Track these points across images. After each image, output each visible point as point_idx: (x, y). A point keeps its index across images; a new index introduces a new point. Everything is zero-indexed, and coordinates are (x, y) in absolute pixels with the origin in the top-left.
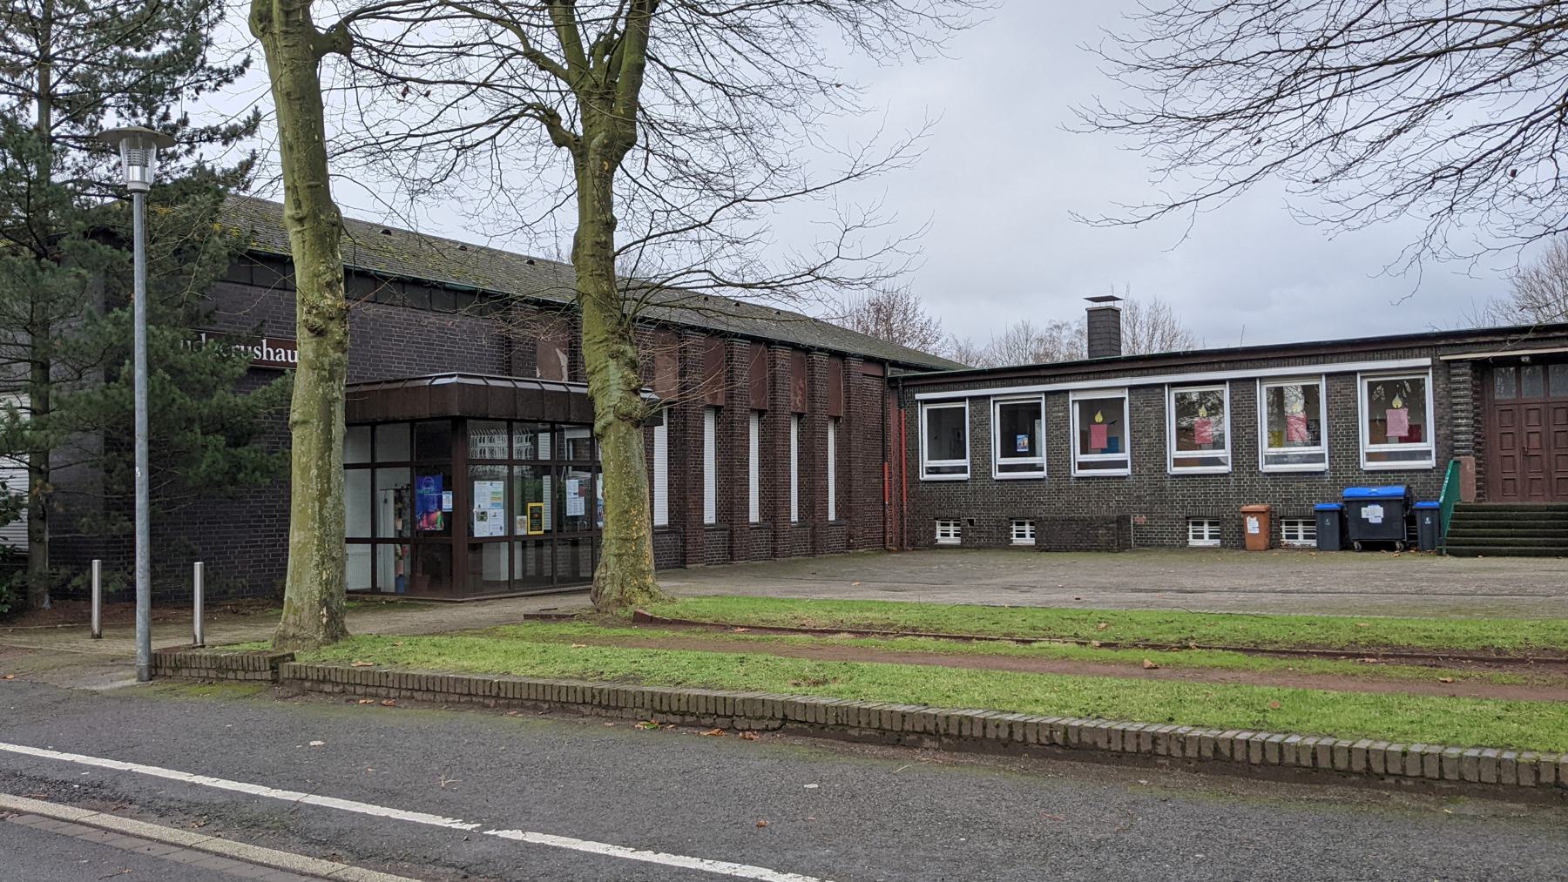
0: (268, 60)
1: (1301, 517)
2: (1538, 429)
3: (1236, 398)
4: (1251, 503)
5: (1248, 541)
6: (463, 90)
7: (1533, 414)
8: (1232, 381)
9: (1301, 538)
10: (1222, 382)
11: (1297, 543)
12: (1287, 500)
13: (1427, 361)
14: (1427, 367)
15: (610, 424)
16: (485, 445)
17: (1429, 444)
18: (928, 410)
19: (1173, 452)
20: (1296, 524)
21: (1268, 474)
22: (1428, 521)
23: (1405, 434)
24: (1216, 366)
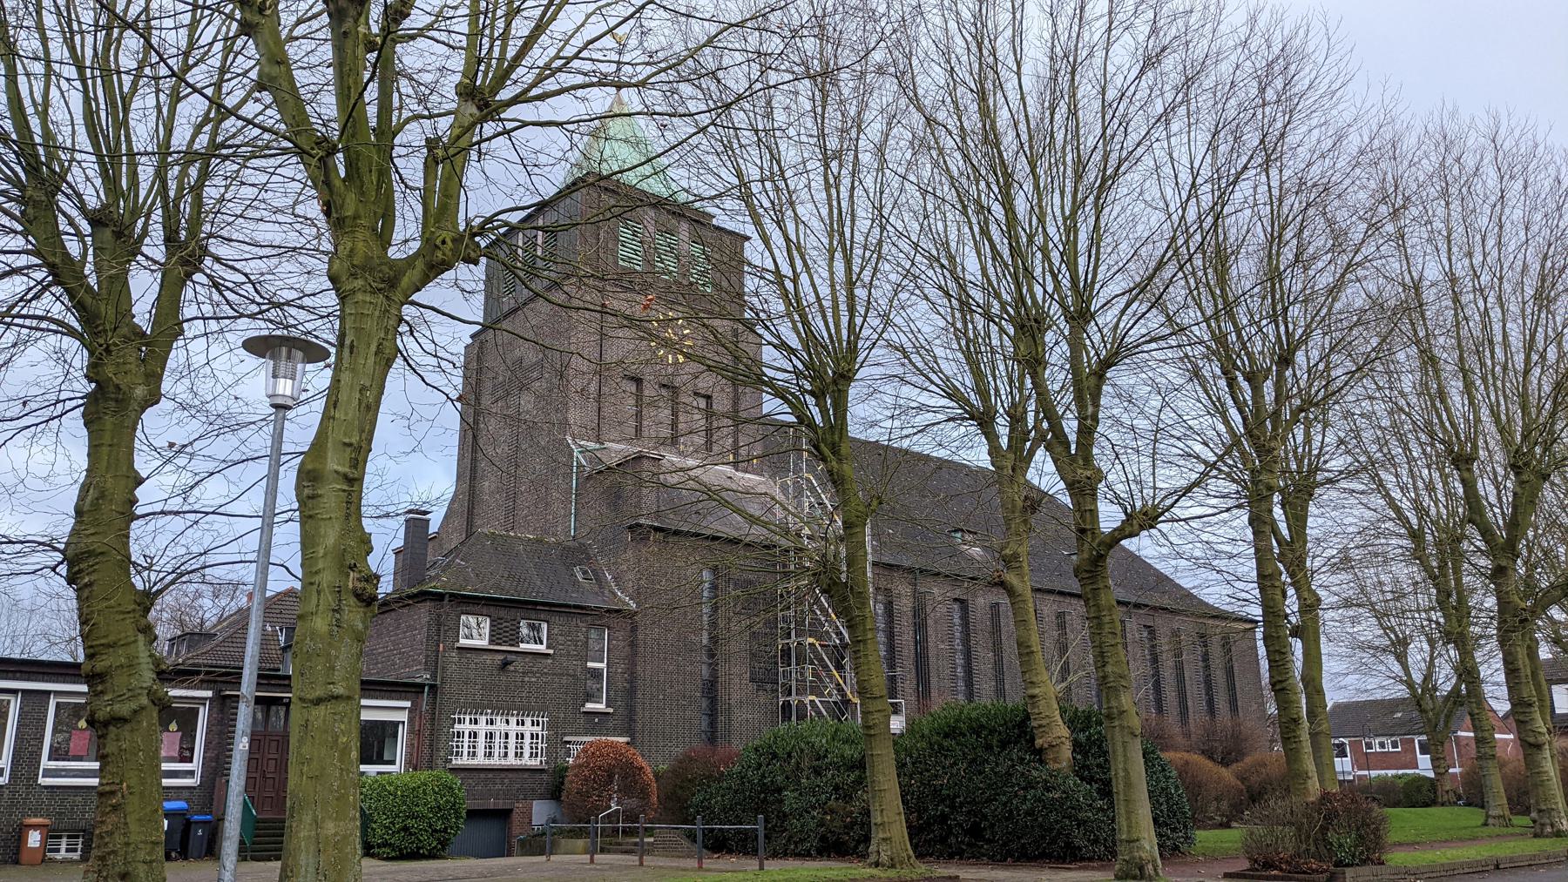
0: (89, 455)
1: (66, 831)
2: (276, 756)
3: (26, 709)
4: (36, 816)
5: (24, 857)
6: (228, 509)
7: (274, 744)
8: (24, 692)
9: (63, 852)
10: (14, 692)
11: (58, 856)
12: (60, 814)
13: (209, 694)
14: (206, 699)
15: (143, 708)
16: (525, 728)
17: (196, 765)
18: (58, 704)
19: (45, 763)
20: (60, 837)
21: (46, 787)
22: (200, 833)
23: (176, 754)
24: (10, 675)
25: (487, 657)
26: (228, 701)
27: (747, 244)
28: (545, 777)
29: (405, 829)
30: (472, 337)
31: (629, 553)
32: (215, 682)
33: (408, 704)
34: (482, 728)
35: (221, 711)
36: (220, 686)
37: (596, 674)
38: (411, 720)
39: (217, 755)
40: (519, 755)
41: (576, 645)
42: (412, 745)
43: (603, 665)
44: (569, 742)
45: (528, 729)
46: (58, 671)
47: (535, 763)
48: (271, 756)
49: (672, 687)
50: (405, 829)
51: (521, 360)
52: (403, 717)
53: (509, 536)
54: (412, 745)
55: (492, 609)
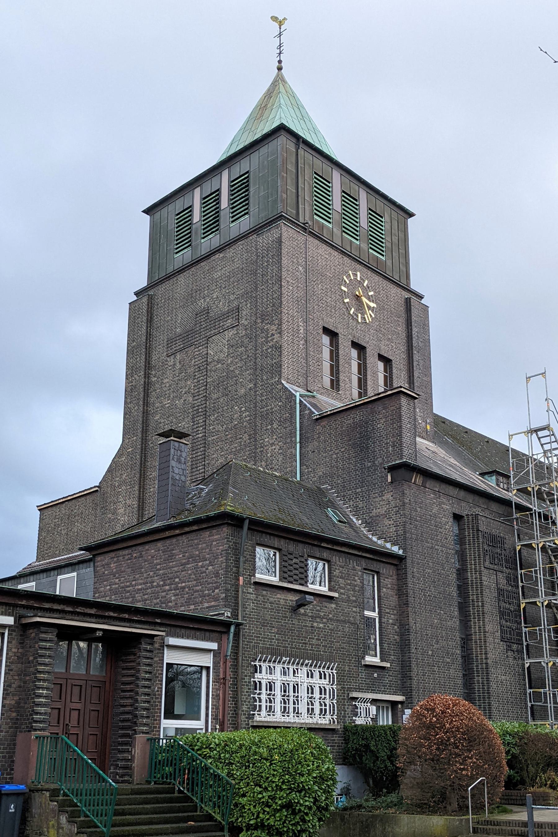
2: (79, 706)
7: (76, 690)
25: (280, 596)
26: (32, 633)
27: (410, 220)
28: (336, 738)
29: (289, 806)
30: (137, 294)
31: (388, 496)
32: (15, 606)
33: (214, 646)
34: (278, 678)
35: (22, 643)
36: (22, 612)
37: (370, 622)
38: (216, 664)
39: (18, 703)
40: (311, 712)
41: (354, 590)
42: (218, 695)
43: (374, 615)
44: (355, 699)
45: (317, 681)
46: (125, 545)
47: (324, 721)
48: (74, 706)
49: (437, 642)
50: (289, 806)
51: (207, 311)
52: (207, 661)
53: (259, 470)
54: (218, 695)
55: (283, 541)
